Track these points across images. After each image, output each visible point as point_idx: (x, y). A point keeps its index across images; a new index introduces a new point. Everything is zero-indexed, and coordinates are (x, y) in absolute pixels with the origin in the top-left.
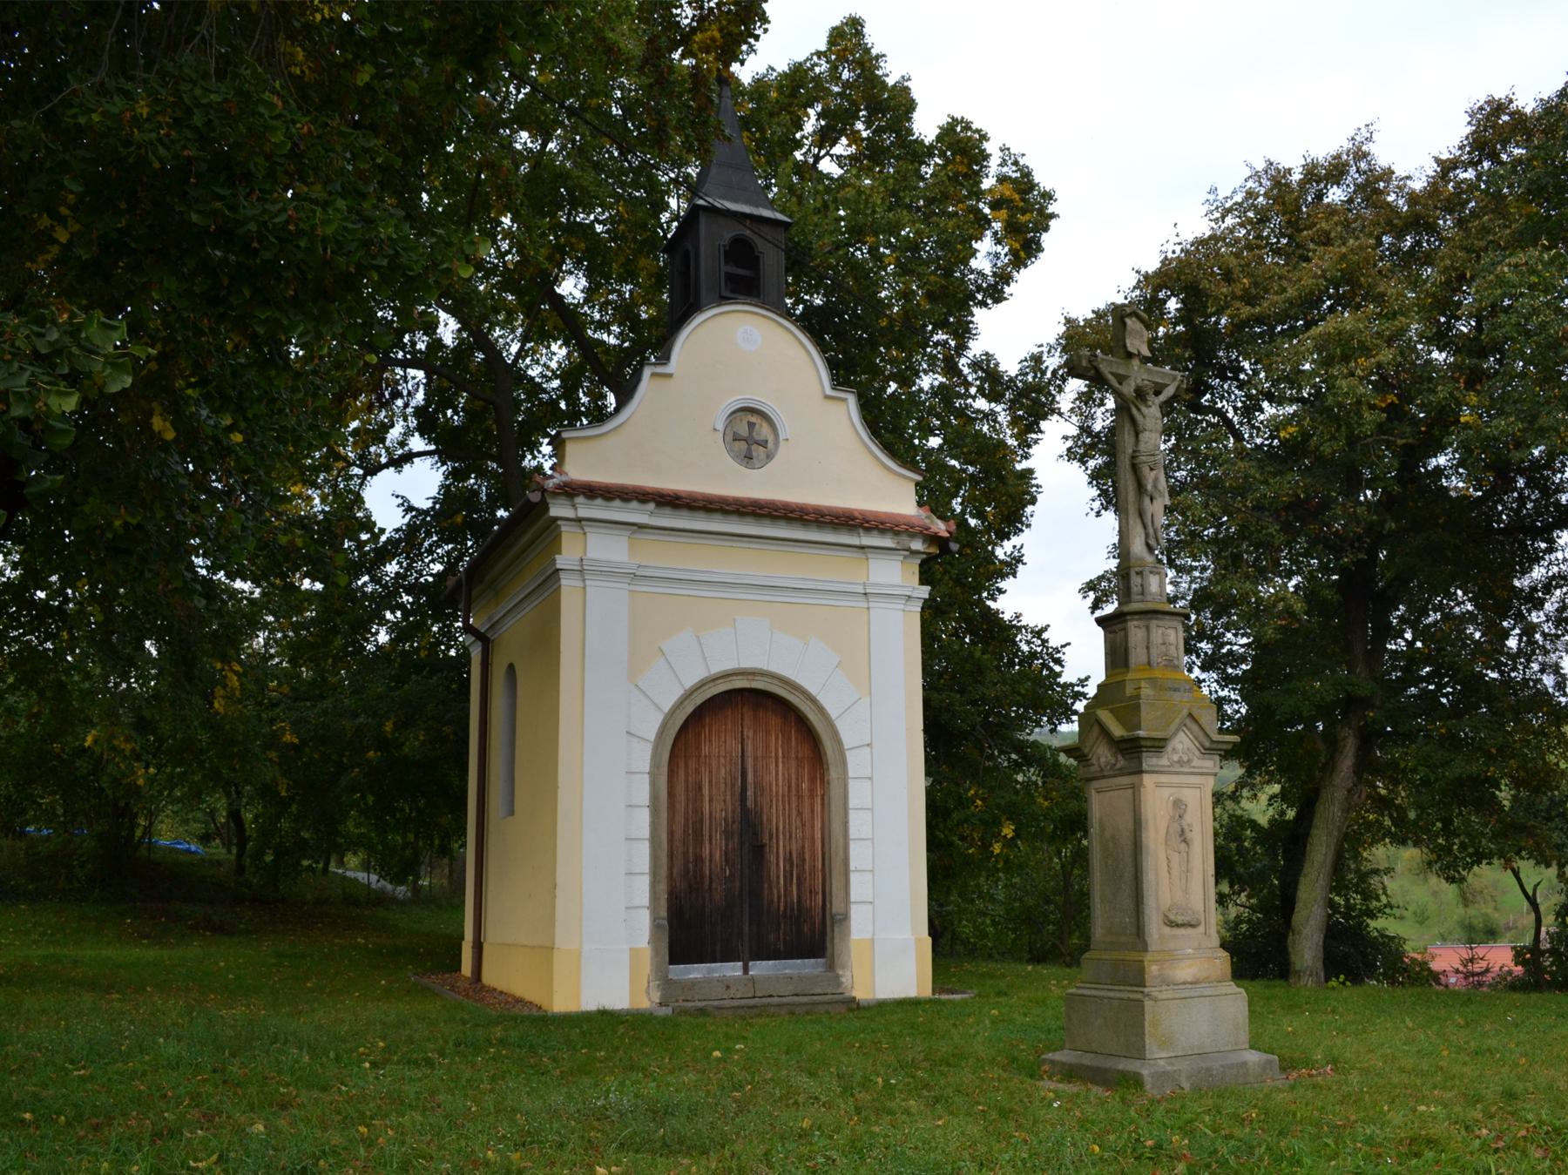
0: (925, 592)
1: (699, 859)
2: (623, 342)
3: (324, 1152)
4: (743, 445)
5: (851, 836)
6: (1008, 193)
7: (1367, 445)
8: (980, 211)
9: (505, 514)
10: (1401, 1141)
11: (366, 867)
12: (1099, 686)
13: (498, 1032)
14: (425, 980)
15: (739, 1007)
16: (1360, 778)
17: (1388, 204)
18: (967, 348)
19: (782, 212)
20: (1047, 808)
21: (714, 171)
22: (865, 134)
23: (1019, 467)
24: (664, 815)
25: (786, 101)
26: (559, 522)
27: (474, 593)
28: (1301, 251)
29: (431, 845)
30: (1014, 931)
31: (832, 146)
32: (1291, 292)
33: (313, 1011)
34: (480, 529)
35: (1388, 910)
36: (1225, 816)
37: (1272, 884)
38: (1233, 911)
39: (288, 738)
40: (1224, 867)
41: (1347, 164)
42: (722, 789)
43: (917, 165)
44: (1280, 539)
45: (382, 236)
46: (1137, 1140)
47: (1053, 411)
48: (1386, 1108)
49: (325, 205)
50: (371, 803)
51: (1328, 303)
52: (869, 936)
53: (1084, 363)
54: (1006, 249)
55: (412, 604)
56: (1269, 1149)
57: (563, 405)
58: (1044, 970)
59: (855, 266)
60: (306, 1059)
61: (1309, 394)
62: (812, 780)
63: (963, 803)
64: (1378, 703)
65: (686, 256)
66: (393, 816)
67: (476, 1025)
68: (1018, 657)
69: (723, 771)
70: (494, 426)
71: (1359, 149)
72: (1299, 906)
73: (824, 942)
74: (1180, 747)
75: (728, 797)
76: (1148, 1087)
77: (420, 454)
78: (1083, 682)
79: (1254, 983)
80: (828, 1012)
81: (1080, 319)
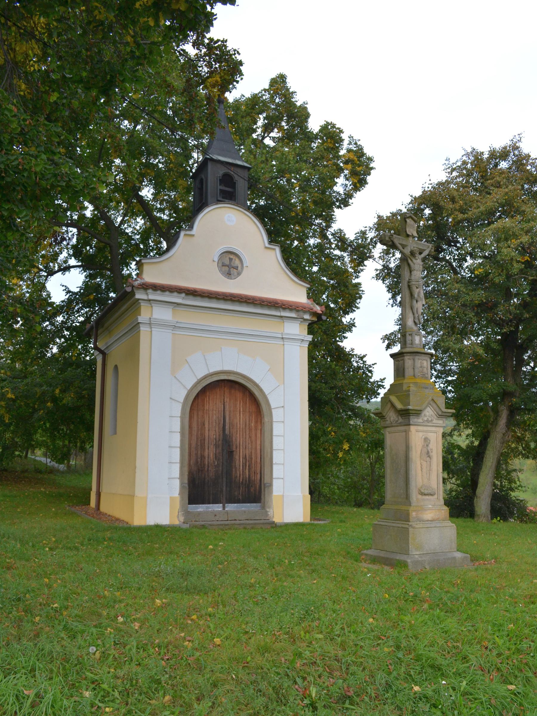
0: (310, 338)
1: (203, 457)
2: (170, 218)
3: (28, 591)
4: (227, 268)
5: (274, 448)
6: (352, 157)
7: (515, 279)
8: (339, 165)
9: (114, 296)
10: (526, 596)
11: (45, 455)
12: (391, 385)
13: (108, 534)
14: (73, 509)
15: (221, 525)
16: (508, 429)
17: (528, 170)
18: (331, 227)
19: (246, 162)
20: (364, 437)
21: (215, 143)
22: (286, 128)
23: (354, 282)
24: (187, 436)
25: (250, 111)
27: (99, 332)
28: (487, 190)
29: (76, 446)
30: (348, 492)
31: (270, 133)
32: (482, 208)
33: (21, 523)
34: (102, 301)
35: (520, 488)
36: (446, 443)
37: (467, 474)
38: (449, 486)
39: (10, 396)
40: (446, 466)
41: (509, 152)
43: (310, 143)
44: (474, 320)
45: (63, 172)
46: (406, 593)
47: (370, 257)
48: (519, 580)
49: (36, 157)
50: (48, 426)
51: (498, 214)
52: (281, 494)
53: (387, 239)
54: (351, 183)
55: (69, 335)
56: (466, 598)
57: (142, 246)
58: (363, 511)
59: (280, 188)
60: (19, 546)
61: (489, 254)
62: (256, 422)
63: (325, 433)
64: (518, 395)
65: (201, 181)
66: (58, 432)
67: (97, 531)
68: (352, 368)
69: (215, 417)
70: (109, 255)
71: (515, 145)
72: (479, 485)
73: (260, 497)
74: (427, 414)
75: (217, 429)
76: (410, 567)
77: (73, 267)
78: (382, 380)
79: (458, 519)
80: (262, 528)
81: (385, 216)
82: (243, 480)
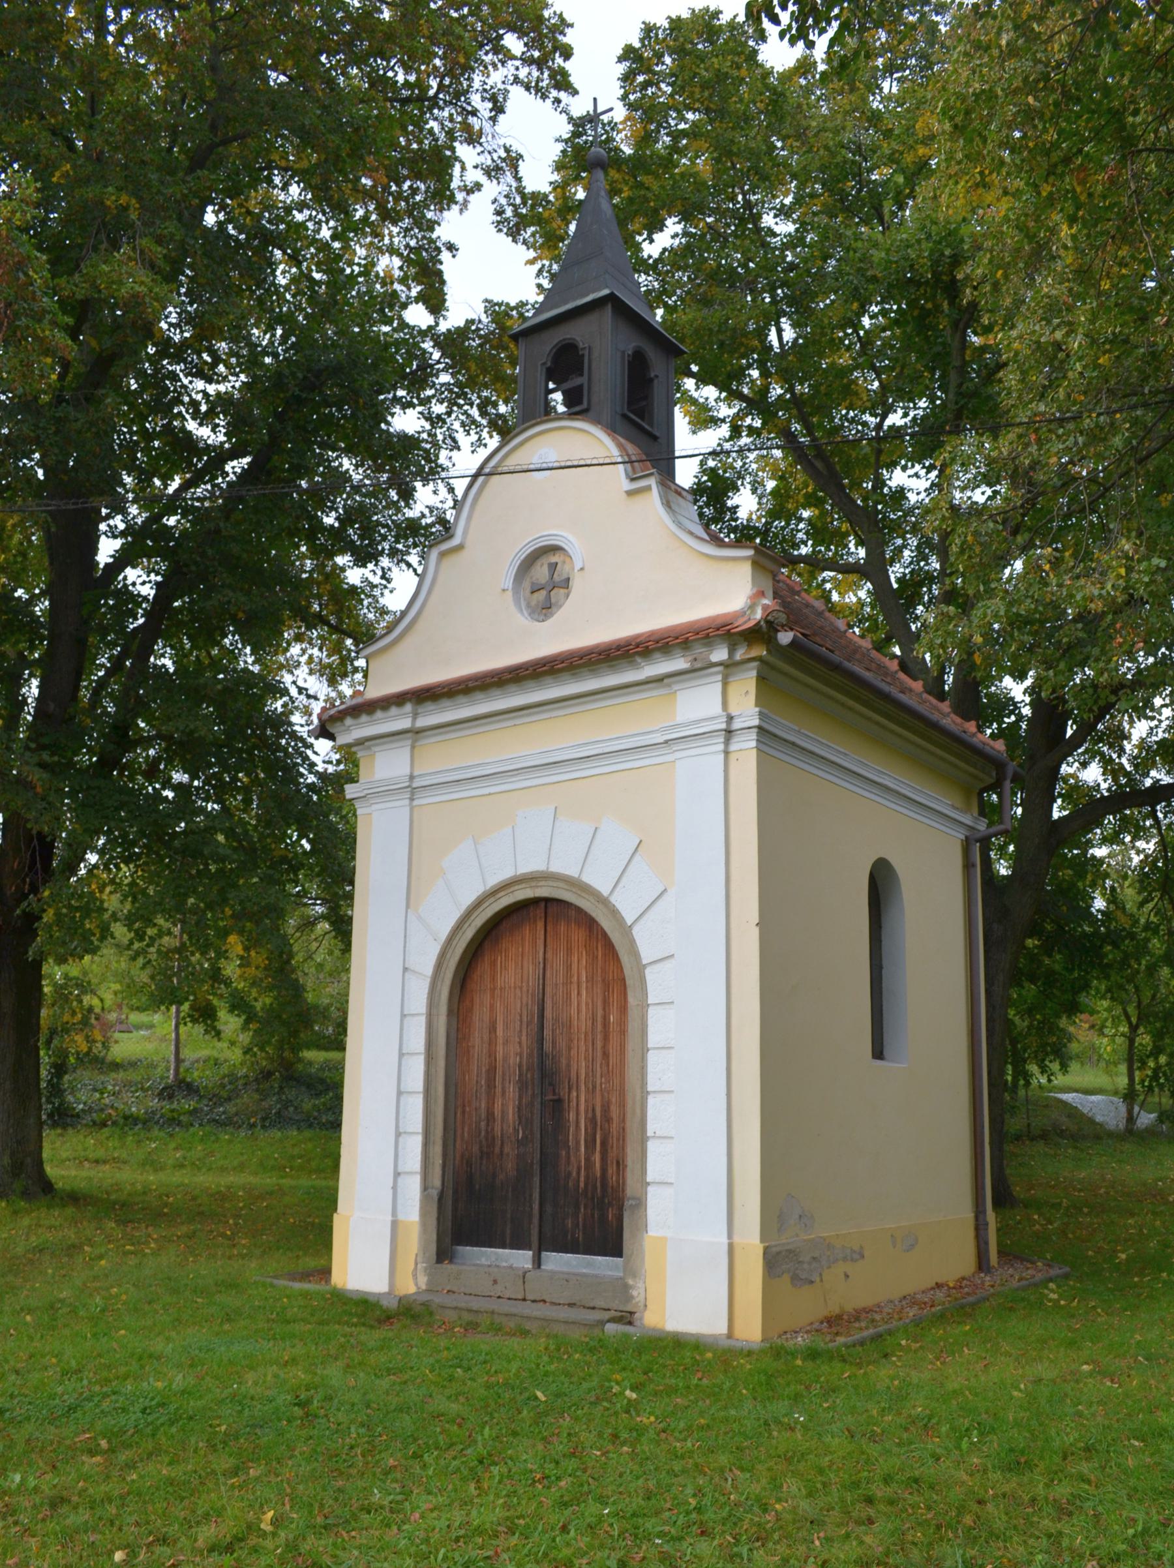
26: (354, 749)
42: (518, 1028)
82: (586, 1184)
